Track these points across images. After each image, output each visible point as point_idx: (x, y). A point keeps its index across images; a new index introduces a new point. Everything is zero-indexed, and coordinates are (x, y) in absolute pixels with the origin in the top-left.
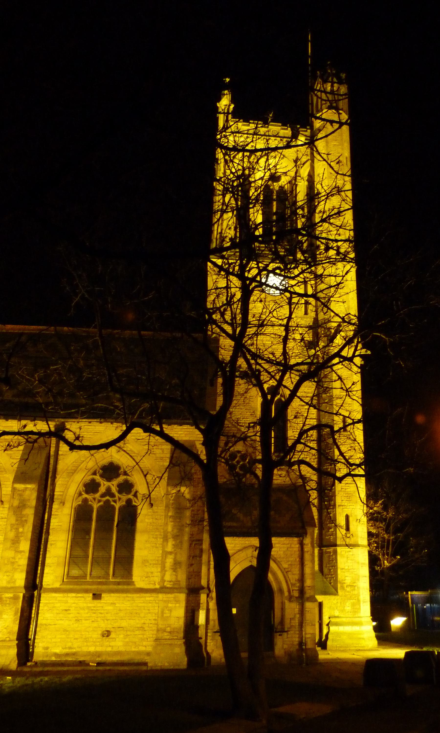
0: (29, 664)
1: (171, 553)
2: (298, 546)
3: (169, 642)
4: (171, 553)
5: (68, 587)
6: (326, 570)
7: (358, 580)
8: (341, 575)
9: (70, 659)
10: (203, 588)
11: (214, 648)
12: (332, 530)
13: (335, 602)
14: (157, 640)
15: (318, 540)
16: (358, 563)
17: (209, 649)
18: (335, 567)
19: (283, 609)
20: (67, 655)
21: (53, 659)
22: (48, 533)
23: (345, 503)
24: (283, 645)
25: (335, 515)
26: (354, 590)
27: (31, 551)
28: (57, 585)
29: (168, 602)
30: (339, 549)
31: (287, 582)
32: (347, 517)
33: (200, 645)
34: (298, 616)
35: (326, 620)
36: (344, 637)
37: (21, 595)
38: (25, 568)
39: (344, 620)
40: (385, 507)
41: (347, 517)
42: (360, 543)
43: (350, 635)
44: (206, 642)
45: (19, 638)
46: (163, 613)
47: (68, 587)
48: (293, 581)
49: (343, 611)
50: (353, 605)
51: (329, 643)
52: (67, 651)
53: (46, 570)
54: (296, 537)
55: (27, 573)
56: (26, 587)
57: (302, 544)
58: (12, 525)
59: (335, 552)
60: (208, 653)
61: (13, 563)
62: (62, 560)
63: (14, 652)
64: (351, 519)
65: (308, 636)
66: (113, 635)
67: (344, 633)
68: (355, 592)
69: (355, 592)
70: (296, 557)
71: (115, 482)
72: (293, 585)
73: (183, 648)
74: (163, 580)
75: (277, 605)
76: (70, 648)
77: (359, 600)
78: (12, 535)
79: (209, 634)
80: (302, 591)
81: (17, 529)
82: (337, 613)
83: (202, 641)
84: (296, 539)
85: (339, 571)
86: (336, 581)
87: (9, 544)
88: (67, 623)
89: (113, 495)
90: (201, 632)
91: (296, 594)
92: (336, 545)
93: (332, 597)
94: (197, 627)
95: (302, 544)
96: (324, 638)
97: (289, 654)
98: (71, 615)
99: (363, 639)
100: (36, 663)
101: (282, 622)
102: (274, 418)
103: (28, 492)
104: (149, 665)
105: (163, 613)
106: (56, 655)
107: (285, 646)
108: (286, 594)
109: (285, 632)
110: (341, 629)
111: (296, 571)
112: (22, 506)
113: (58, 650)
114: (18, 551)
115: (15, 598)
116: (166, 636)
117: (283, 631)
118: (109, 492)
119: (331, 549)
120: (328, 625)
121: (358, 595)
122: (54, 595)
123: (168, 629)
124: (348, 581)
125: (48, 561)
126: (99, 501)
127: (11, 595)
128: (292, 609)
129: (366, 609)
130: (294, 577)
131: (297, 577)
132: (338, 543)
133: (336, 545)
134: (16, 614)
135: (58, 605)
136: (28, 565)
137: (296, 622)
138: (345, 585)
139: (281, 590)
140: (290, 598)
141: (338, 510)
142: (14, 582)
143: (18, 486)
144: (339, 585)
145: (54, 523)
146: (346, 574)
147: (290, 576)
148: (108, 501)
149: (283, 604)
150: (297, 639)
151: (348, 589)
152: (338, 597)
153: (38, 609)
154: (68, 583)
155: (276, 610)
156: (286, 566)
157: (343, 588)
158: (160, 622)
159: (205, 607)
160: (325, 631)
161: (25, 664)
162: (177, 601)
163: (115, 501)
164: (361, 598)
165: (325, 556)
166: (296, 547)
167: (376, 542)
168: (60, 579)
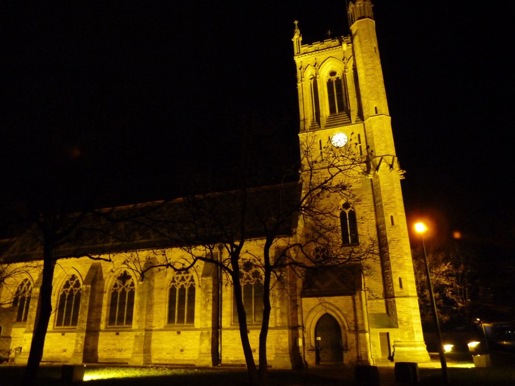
0: (219, 365)
1: (278, 308)
2: (351, 301)
3: (281, 355)
4: (278, 308)
5: (234, 327)
6: (390, 313)
7: (411, 318)
8: (399, 315)
9: (237, 363)
10: (299, 326)
11: (310, 359)
12: (391, 288)
13: (397, 332)
14: (276, 354)
15: (236, 306)
16: (410, 307)
17: (306, 359)
18: (395, 310)
19: (346, 337)
20: (237, 361)
21: (230, 363)
22: (222, 301)
23: (397, 270)
24: (348, 357)
25: (392, 278)
26: (409, 324)
27: (213, 310)
28: (228, 326)
29: (279, 334)
30: (396, 299)
31: (347, 321)
32: (400, 279)
33: (301, 357)
34: (355, 341)
35: (392, 343)
36: (405, 354)
37: (211, 332)
38: (211, 318)
39: (404, 343)
40: (456, 267)
41: (400, 279)
42: (410, 295)
43: (409, 353)
44: (304, 356)
45: (212, 353)
46: (277, 340)
47: (234, 327)
48: (351, 321)
49: (402, 338)
50: (409, 334)
51: (395, 358)
52: (236, 359)
53: (223, 319)
54: (350, 295)
55: (213, 321)
56: (213, 328)
57: (354, 300)
58: (203, 298)
59: (394, 301)
60: (306, 362)
61: (206, 316)
62: (229, 314)
63: (210, 359)
64: (402, 280)
65: (362, 353)
66: (181, 348)
67: (404, 352)
68: (410, 326)
69: (410, 326)
70: (351, 307)
71: (251, 272)
72: (350, 323)
73: (289, 358)
74: (276, 323)
75: (343, 335)
76: (237, 358)
77: (413, 331)
78: (204, 302)
79: (306, 351)
80: (356, 327)
81: (206, 299)
82: (399, 339)
83: (302, 355)
84: (350, 297)
85: (398, 313)
86: (397, 319)
87: (203, 307)
88: (234, 345)
89: (250, 279)
90: (301, 350)
91: (353, 329)
92: (394, 297)
93: (395, 329)
94: (298, 348)
95: (354, 300)
96: (392, 354)
97: (351, 363)
98: (237, 341)
99: (418, 355)
100: (222, 365)
101: (346, 345)
102: (349, 221)
103: (208, 281)
104: (273, 367)
105: (277, 340)
106: (231, 361)
107: (349, 359)
108: (347, 329)
109: (348, 350)
110: (402, 349)
111: (352, 315)
112: (207, 288)
113: (232, 359)
114: (207, 310)
115: (208, 333)
116: (280, 352)
117: (347, 350)
118: (248, 278)
119: (392, 300)
120: (393, 346)
121: (412, 327)
122: (228, 331)
123: (281, 348)
124: (404, 319)
125: (223, 314)
126: (244, 282)
127: (206, 332)
128: (351, 337)
129: (419, 337)
130: (351, 318)
131: (353, 319)
132: (396, 295)
133: (394, 297)
134: (209, 341)
135: (230, 336)
136: (213, 317)
137: (354, 345)
138: (403, 322)
139: (344, 327)
140: (350, 331)
141: (393, 275)
142: (207, 325)
143: (203, 278)
144: (399, 322)
145: (224, 295)
146: (403, 315)
147: (349, 319)
148: (248, 282)
149: (346, 334)
150: (356, 355)
151: (405, 324)
152: (398, 329)
153: (221, 338)
154: (234, 325)
155: (343, 339)
156: (345, 313)
157: (401, 323)
158: (277, 345)
159: (302, 336)
160: (392, 351)
161: (217, 365)
162: (284, 334)
163: (252, 282)
164: (415, 329)
165: (389, 304)
166: (351, 301)
167: (451, 291)
168: (230, 323)
